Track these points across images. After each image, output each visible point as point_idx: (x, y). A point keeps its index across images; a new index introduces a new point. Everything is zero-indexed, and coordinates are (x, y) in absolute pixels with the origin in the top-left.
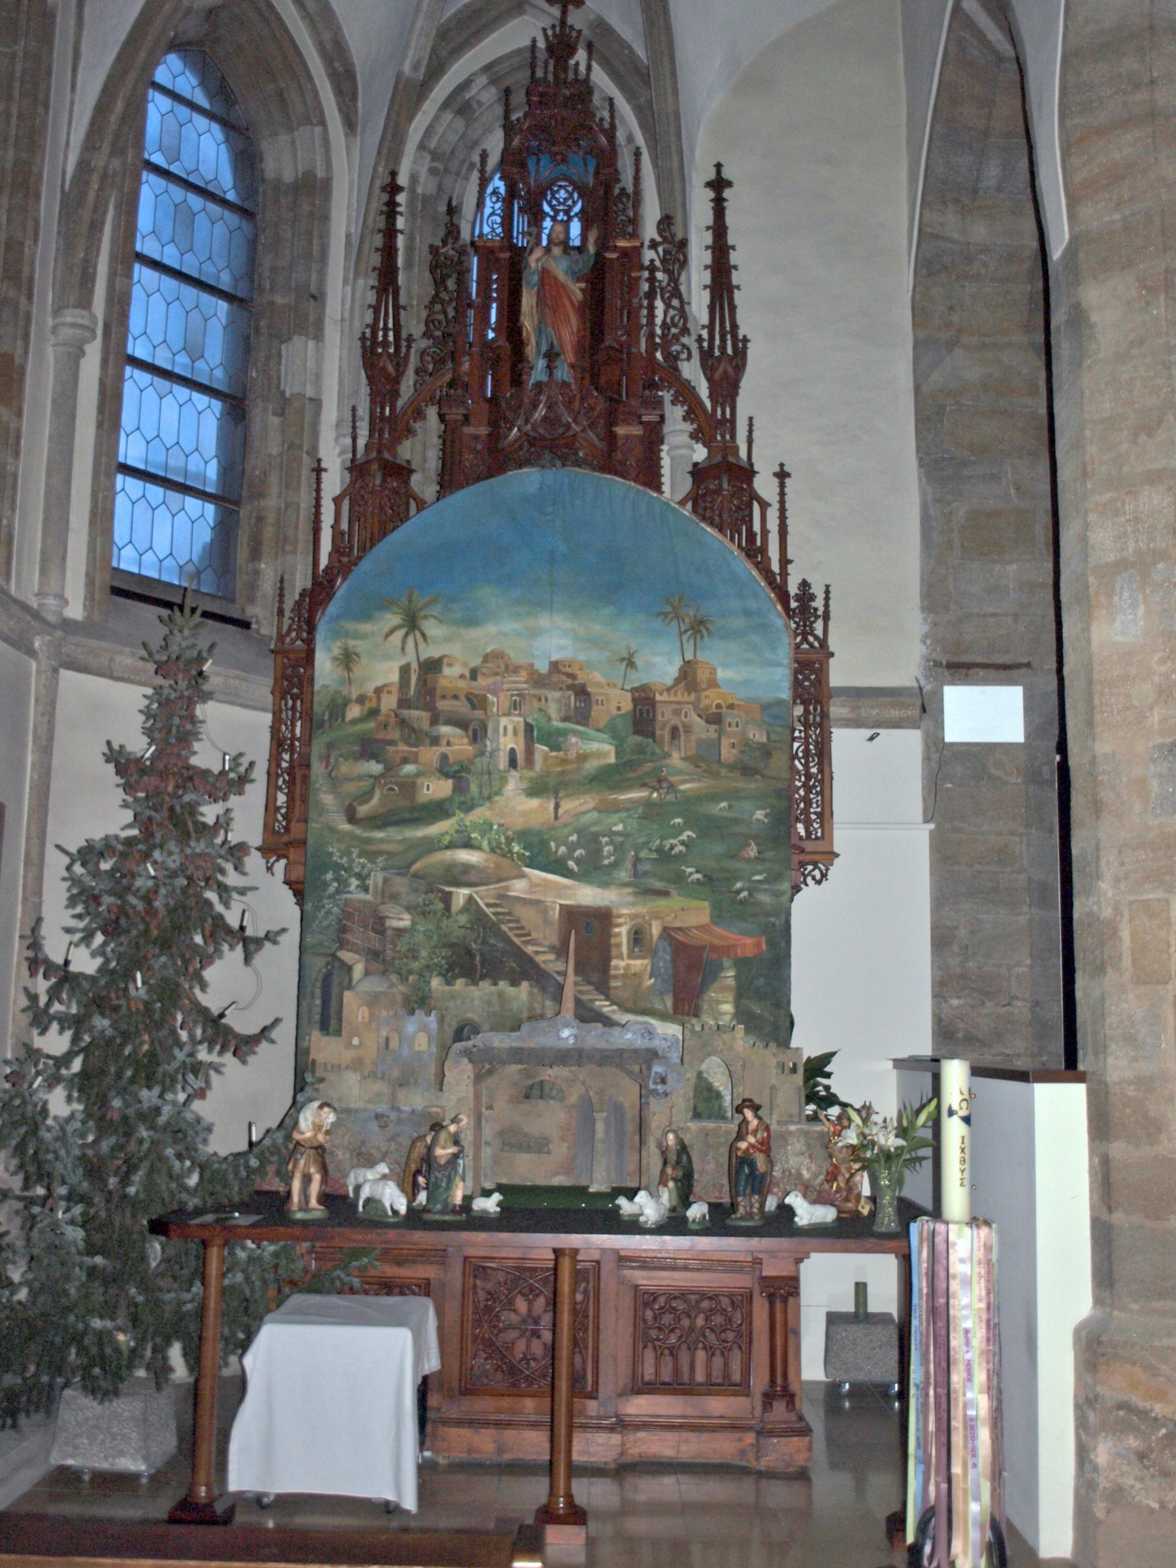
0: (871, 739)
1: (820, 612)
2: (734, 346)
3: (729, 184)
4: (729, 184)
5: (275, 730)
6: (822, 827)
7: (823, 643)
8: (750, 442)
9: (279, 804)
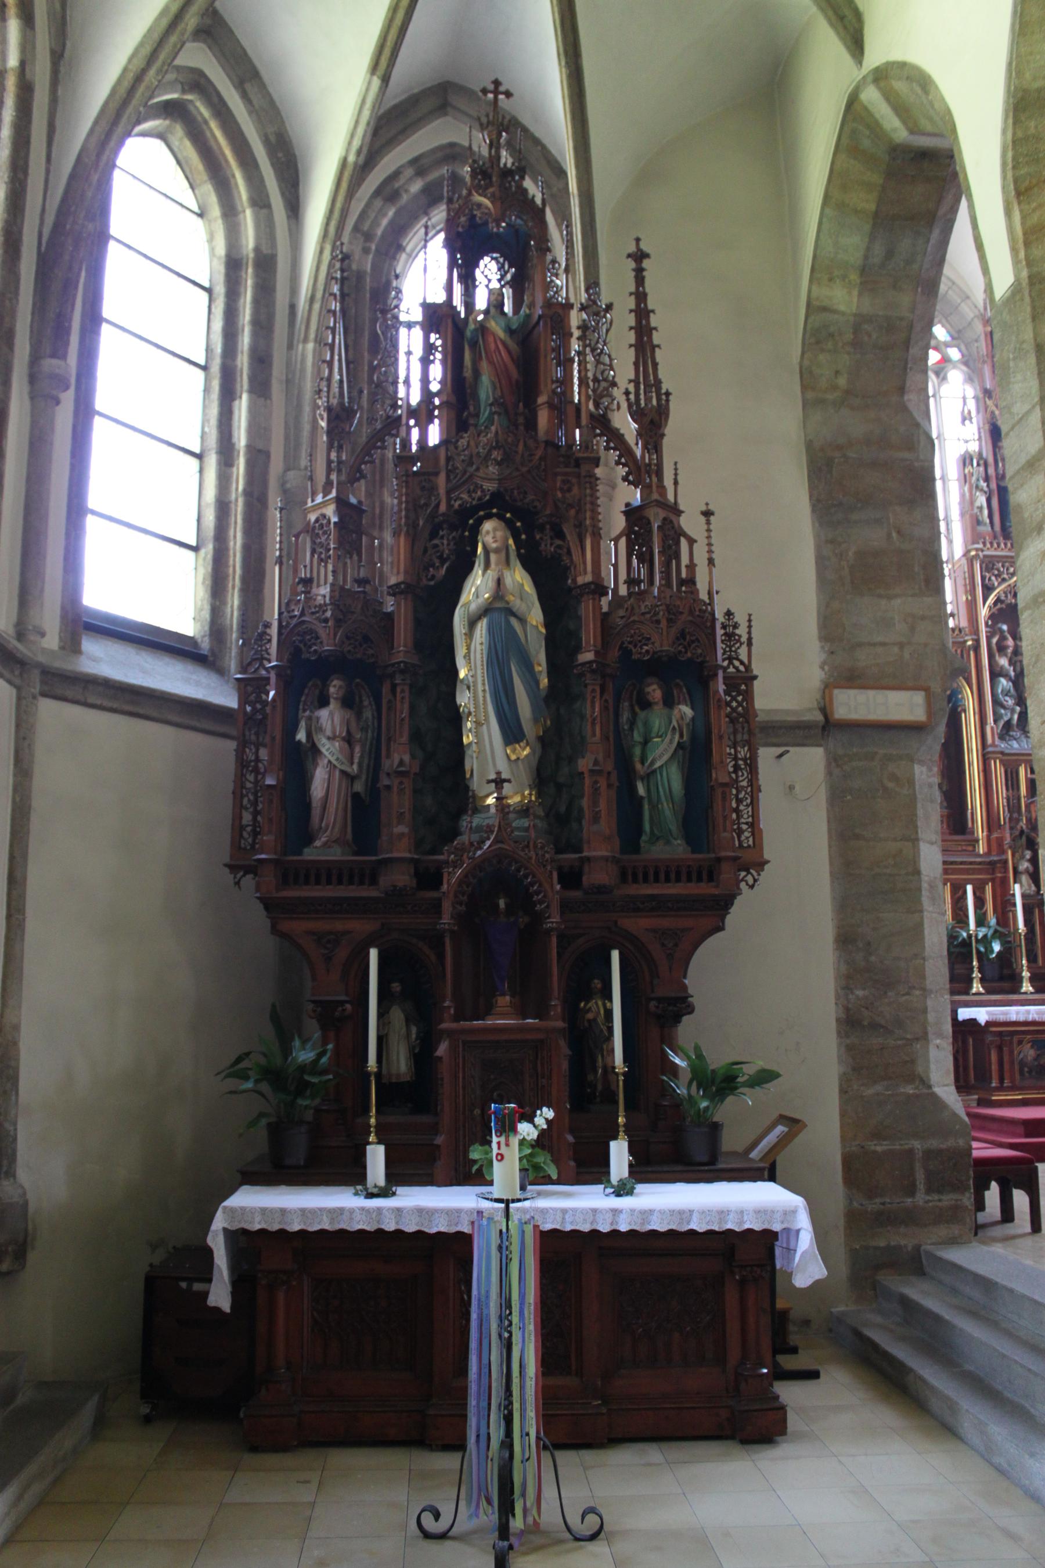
0: (781, 756)
1: (744, 639)
2: (659, 399)
3: (647, 256)
4: (647, 256)
5: (240, 753)
6: (753, 834)
7: (748, 668)
8: (676, 483)
9: (244, 822)
